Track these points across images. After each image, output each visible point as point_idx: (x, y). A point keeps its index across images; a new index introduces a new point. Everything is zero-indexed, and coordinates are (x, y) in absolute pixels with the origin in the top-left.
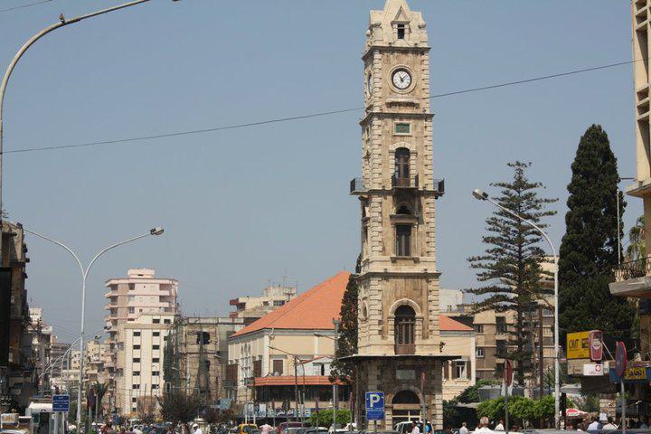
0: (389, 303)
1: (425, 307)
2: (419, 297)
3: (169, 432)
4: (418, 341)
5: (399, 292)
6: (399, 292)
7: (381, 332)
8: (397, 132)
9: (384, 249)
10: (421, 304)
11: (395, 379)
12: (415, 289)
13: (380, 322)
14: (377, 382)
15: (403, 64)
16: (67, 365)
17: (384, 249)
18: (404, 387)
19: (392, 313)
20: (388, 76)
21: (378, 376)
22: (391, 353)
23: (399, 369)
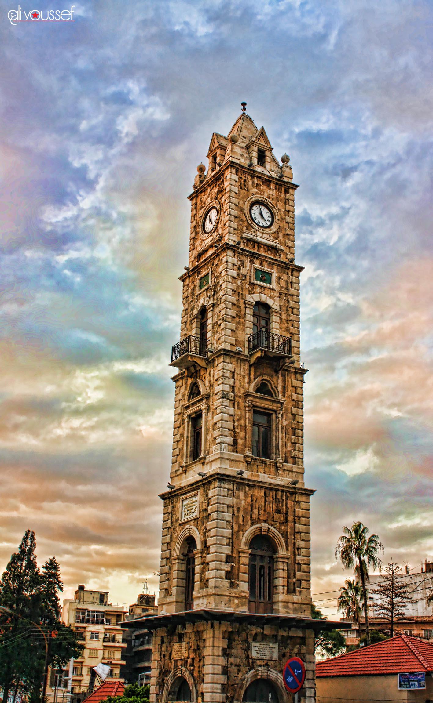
0: (242, 528)
1: (291, 542)
2: (281, 524)
3: (117, 701)
4: (281, 596)
5: (256, 511)
6: (256, 511)
7: (229, 575)
8: (256, 279)
9: (235, 443)
10: (285, 535)
11: (248, 657)
12: (278, 511)
13: (229, 559)
14: (222, 661)
15: (264, 197)
16: (122, 241)
17: (235, 443)
18: (262, 672)
19: (245, 544)
20: (247, 205)
21: (224, 650)
22: (244, 610)
23: (254, 640)
